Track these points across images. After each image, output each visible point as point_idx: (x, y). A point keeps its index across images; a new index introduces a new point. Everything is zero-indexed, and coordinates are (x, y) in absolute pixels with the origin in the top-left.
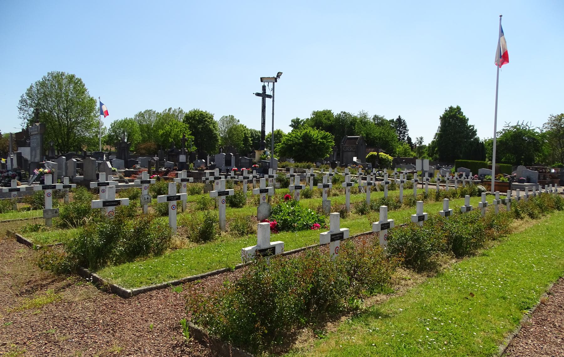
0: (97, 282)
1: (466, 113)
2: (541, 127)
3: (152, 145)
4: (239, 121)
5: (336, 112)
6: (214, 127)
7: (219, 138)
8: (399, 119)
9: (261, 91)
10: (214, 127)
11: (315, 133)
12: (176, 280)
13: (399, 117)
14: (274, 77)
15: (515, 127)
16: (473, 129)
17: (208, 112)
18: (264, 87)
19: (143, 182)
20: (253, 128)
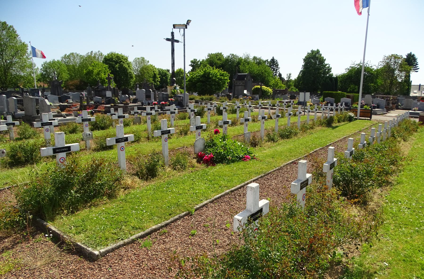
0: (57, 239)
1: (324, 54)
2: (377, 65)
3: (77, 81)
4: (148, 62)
5: (226, 55)
6: (129, 67)
7: (134, 76)
8: (273, 60)
9: (170, 37)
10: (129, 67)
11: (216, 72)
12: (142, 233)
13: (273, 57)
14: (184, 24)
15: (359, 65)
16: (329, 67)
17: (123, 54)
18: (172, 33)
19: (83, 120)
20: (160, 68)
